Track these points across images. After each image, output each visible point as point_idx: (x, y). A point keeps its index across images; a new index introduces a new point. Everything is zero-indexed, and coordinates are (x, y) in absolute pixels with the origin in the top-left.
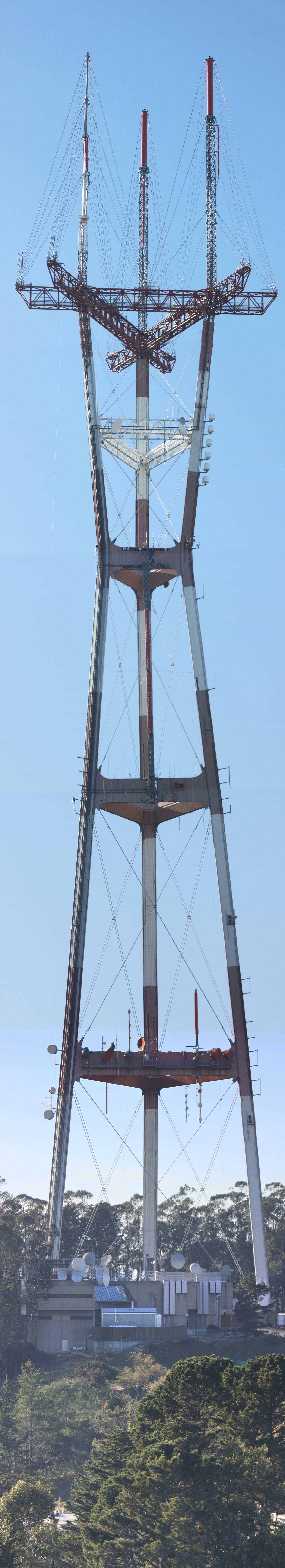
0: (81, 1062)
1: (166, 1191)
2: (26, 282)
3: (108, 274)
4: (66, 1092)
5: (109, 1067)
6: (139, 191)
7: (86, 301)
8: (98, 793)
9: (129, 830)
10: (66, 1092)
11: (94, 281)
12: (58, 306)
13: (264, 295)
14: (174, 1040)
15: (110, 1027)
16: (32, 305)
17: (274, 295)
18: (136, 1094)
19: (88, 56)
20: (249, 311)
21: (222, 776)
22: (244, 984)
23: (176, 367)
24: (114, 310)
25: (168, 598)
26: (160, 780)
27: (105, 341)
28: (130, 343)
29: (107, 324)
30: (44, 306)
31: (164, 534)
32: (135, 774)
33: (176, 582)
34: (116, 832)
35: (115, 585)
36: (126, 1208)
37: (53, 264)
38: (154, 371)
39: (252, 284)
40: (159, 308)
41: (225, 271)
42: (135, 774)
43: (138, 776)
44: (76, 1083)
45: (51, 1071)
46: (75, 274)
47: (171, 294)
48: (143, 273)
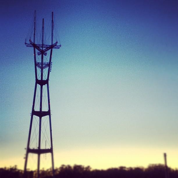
0: (29, 151)
1: (41, 168)
2: (26, 43)
3: (38, 42)
4: (26, 158)
5: (33, 151)
6: (42, 30)
7: (35, 46)
8: (34, 113)
9: (38, 118)
10: (26, 158)
11: (36, 43)
12: (31, 46)
13: (59, 46)
14: (43, 147)
15: (34, 145)
16: (27, 46)
17: (61, 46)
18: (38, 118)
19: (35, 11)
20: (57, 48)
21: (51, 111)
22: (53, 145)
23: (47, 55)
24: (39, 47)
25: (45, 87)
26: (43, 112)
27: (37, 51)
28: (41, 52)
29: (38, 49)
30: (29, 46)
31: (45, 78)
32: (39, 111)
33: (46, 85)
34: (36, 118)
35: (38, 85)
36: (35, 171)
37: (30, 41)
38: (44, 56)
39: (58, 44)
40: (45, 47)
41: (54, 42)
42: (39, 111)
43: (41, 80)
44: (43, 86)
45: (25, 152)
46: (33, 42)
47: (46, 45)
48: (43, 42)
